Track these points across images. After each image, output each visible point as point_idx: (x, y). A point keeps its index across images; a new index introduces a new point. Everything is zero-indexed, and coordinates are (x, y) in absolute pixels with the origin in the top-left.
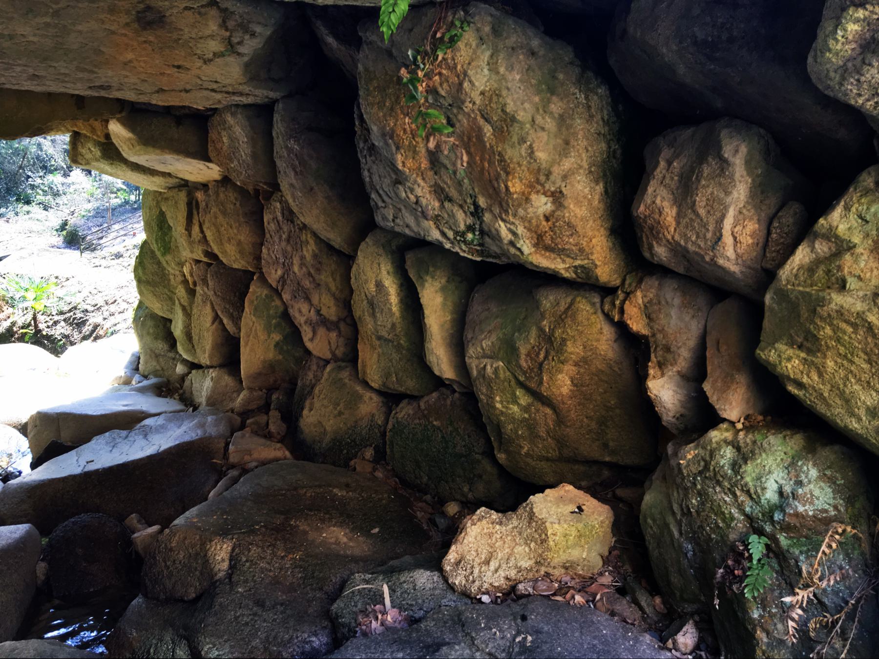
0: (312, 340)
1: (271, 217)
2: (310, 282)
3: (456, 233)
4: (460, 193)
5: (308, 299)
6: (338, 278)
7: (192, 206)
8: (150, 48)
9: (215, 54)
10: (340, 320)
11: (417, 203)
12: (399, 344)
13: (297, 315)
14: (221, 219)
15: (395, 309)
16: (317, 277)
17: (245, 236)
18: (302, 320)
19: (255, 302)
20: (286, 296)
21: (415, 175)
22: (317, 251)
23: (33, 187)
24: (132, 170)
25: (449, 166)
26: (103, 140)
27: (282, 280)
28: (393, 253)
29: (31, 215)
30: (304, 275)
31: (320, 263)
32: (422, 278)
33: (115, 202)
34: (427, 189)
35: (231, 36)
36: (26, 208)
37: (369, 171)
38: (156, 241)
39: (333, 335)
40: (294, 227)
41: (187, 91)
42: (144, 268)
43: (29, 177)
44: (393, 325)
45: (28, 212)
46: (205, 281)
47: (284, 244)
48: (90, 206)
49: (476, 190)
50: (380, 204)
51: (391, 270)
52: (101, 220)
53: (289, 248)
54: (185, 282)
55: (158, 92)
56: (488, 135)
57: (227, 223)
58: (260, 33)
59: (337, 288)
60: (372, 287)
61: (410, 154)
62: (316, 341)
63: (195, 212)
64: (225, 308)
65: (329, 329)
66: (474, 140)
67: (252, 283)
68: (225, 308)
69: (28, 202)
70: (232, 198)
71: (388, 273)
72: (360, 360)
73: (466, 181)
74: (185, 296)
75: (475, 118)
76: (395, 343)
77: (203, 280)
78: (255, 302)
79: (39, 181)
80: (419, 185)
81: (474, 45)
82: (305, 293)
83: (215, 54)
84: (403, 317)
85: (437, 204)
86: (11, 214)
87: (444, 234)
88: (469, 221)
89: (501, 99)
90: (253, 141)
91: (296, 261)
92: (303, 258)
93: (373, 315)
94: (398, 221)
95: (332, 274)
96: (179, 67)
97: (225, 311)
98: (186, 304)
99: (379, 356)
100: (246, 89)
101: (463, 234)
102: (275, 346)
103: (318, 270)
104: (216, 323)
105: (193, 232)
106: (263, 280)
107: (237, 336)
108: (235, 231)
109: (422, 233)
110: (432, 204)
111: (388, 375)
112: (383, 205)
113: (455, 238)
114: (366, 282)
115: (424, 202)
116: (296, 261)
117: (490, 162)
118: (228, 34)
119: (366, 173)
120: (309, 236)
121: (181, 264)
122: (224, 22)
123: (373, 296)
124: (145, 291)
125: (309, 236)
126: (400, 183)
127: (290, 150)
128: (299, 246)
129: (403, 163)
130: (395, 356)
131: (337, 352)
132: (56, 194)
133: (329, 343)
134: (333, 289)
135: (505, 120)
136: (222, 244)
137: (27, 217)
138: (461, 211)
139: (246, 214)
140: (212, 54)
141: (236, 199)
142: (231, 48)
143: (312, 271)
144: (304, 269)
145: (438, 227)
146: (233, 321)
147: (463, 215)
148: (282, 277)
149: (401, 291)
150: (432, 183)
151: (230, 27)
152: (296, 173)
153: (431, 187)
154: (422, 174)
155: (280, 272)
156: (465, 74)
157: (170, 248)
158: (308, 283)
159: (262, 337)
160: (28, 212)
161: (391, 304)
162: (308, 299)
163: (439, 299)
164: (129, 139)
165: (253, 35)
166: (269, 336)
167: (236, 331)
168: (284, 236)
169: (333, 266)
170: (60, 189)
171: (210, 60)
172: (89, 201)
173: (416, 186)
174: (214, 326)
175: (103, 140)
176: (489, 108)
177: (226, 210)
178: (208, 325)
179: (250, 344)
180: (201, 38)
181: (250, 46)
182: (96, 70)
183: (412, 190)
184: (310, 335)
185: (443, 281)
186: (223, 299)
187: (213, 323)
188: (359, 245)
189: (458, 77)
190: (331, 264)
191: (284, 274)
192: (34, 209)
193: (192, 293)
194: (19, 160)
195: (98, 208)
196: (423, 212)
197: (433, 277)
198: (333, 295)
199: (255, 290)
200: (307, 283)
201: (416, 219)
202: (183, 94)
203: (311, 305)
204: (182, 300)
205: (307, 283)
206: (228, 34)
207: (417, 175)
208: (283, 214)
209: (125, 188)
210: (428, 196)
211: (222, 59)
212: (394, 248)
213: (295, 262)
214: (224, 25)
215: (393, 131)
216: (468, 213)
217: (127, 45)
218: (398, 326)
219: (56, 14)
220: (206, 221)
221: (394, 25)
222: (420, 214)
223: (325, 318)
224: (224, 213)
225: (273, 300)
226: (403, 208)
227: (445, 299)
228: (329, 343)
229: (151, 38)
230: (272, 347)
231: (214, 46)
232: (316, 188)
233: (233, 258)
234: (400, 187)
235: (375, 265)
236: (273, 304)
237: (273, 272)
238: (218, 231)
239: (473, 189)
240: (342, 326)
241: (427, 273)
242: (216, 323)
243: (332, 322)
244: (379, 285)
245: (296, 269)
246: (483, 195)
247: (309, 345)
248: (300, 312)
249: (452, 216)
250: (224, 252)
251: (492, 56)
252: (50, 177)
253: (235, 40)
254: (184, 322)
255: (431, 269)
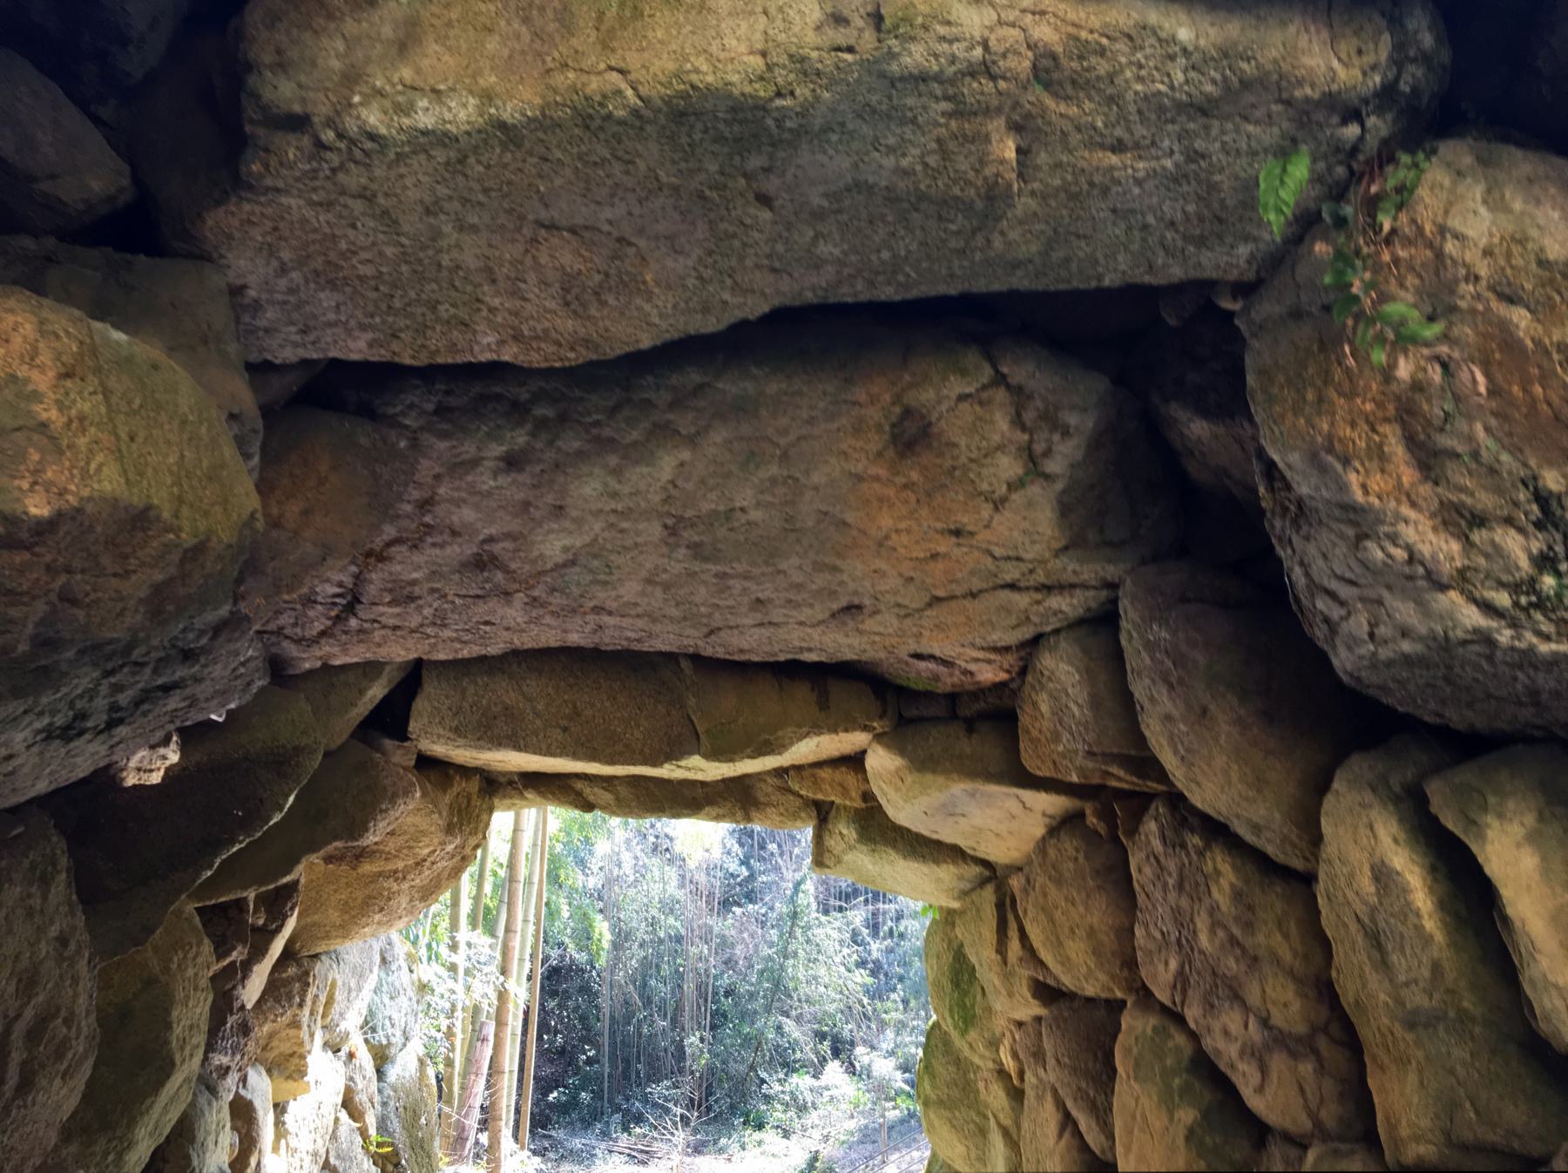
0: (1260, 1090)
1: (1143, 855)
2: (1237, 960)
3: (1515, 588)
4: (1499, 491)
5: (1237, 998)
6: (1293, 929)
7: (1006, 907)
8: (913, 499)
9: (1011, 487)
10: (1315, 1030)
11: (1412, 559)
12: (1461, 1012)
13: (1221, 1044)
14: (1053, 891)
15: (1430, 924)
16: (1248, 942)
17: (1098, 914)
18: (1232, 1050)
19: (1135, 1050)
20: (1192, 1014)
21: (1393, 504)
22: (1239, 884)
23: (768, 1099)
24: (905, 857)
25: (1460, 449)
26: (859, 804)
27: (1182, 982)
28: (1396, 800)
29: (764, 1147)
30: (1222, 946)
31: (1250, 908)
32: (1474, 823)
33: (893, 1115)
34: (1426, 524)
35: (1031, 442)
36: (757, 1135)
37: (1302, 563)
38: (951, 1011)
39: (1307, 1068)
40: (1188, 854)
41: (973, 595)
42: (933, 1076)
43: (763, 1081)
44: (1436, 967)
45: (760, 1143)
46: (1039, 1056)
47: (1172, 896)
48: (852, 1125)
49: (1533, 463)
50: (1336, 613)
51: (1402, 836)
52: (870, 1147)
53: (1184, 902)
54: (1002, 1073)
55: (930, 605)
56: (1523, 324)
57: (1066, 899)
58: (1077, 428)
59: (1295, 954)
60: (1367, 885)
61: (1375, 464)
62: (1270, 1090)
63: (1011, 917)
64: (1079, 1089)
65: (1294, 1055)
66: (1497, 356)
67: (1125, 1012)
68: (1079, 1089)
69: (760, 1126)
70: (1071, 852)
71: (1396, 841)
72: (1379, 1116)
73: (1505, 457)
74: (1007, 1107)
75: (1488, 309)
76: (1452, 1014)
77: (1034, 1055)
78: (1135, 1050)
79: (777, 1087)
80: (1406, 522)
81: (1447, 182)
82: (1230, 987)
83: (1009, 485)
84: (1453, 944)
85: (1455, 547)
86: (735, 1148)
87: (1488, 608)
88: (1536, 546)
89: (1530, 246)
90: (1089, 675)
91: (1202, 923)
92: (1213, 910)
93: (1384, 965)
94: (1382, 631)
95: (1280, 925)
96: (957, 533)
97: (1080, 1095)
98: (1007, 1122)
99: (1420, 1072)
100: (1069, 567)
101: (1532, 585)
102: (1188, 1139)
103: (1249, 926)
104: (1067, 1135)
105: (1010, 954)
106: (1145, 996)
107: (1109, 1157)
108: (1081, 909)
109: (1439, 630)
110: (1444, 550)
111: (1449, 1108)
112: (1343, 612)
113: (1516, 604)
114: (1351, 877)
115: (1426, 550)
116: (1202, 923)
117: (1544, 380)
118: (1026, 437)
119: (1298, 573)
120: (1219, 859)
121: (994, 1044)
122: (1018, 415)
123: (1373, 910)
124: (936, 1123)
125: (1219, 859)
126: (1367, 536)
127: (1150, 646)
128: (1203, 888)
129: (1364, 487)
130: (1460, 1053)
131: (1323, 1114)
132: (802, 1109)
133: (1302, 1090)
134: (1286, 955)
135: (1552, 281)
136: (1060, 944)
137: (758, 1150)
138: (1512, 532)
139: (1097, 872)
140: (1004, 487)
141: (1077, 850)
142: (1033, 462)
143: (1236, 931)
144: (1221, 933)
145: (1473, 600)
146: (1098, 1118)
147: (1520, 538)
148: (1180, 973)
149: (1435, 880)
150: (1435, 504)
151: (1028, 424)
152: (1171, 687)
153: (1433, 516)
154: (1408, 496)
155: (1173, 965)
156: (1442, 230)
157: (974, 1016)
158: (1232, 963)
159: (1157, 1121)
160: (760, 1143)
161: (1418, 915)
162: (1237, 998)
163: (1529, 861)
164: (898, 770)
165: (1066, 433)
166: (1171, 1119)
167: (1106, 1144)
168: (1171, 882)
169: (1279, 907)
170: (809, 1099)
171: (1004, 500)
172: (852, 1117)
173: (1401, 527)
174: (1063, 1142)
175: (859, 804)
176: (1509, 271)
177: (1061, 875)
178: (1051, 1141)
179: (1135, 1148)
180: (986, 456)
181: (1063, 456)
182: (838, 562)
183: (1394, 538)
184: (1255, 1078)
185: (1530, 819)
186: (1074, 1070)
187: (1060, 1136)
188: (1320, 804)
189: (1430, 245)
190: (1273, 901)
191: (1183, 967)
192: (770, 1136)
193: (1017, 1095)
194: (749, 1055)
195: (866, 1127)
196: (1429, 574)
197: (1501, 816)
198: (1291, 973)
199: (1135, 1025)
200: (1231, 965)
201: (1421, 604)
202: (967, 603)
203: (1246, 1008)
204: (1001, 1116)
205: (1231, 965)
206: (1026, 437)
207: (1399, 502)
208: (1163, 838)
209: (907, 1088)
210: (1431, 536)
211: (1022, 492)
212: (1397, 789)
213: (1199, 925)
214: (1018, 422)
215: (1330, 438)
216: (1531, 528)
217: (881, 500)
218: (1446, 964)
219: (785, 457)
220: (1030, 907)
221: (1287, 204)
222: (1422, 583)
223: (1280, 1031)
224: (1059, 881)
225: (1170, 1036)
226: (1385, 594)
227: (1544, 859)
228: (1302, 1090)
229: (915, 476)
230: (1181, 1141)
231: (1009, 466)
232: (1212, 707)
233: (1084, 974)
234: (1370, 544)
235: (1363, 832)
236: (1170, 1044)
237: (1161, 967)
238: (1052, 921)
239: (1525, 465)
240: (1322, 1043)
241: (1485, 809)
242: (1067, 1135)
243: (1299, 1039)
244: (1383, 875)
245: (1204, 939)
246: (1551, 464)
247: (1255, 1103)
248: (1226, 1033)
249: (1498, 551)
250: (1066, 962)
251: (1489, 191)
252: (795, 1079)
253: (1039, 448)
254: (1008, 1159)
255: (1492, 800)
